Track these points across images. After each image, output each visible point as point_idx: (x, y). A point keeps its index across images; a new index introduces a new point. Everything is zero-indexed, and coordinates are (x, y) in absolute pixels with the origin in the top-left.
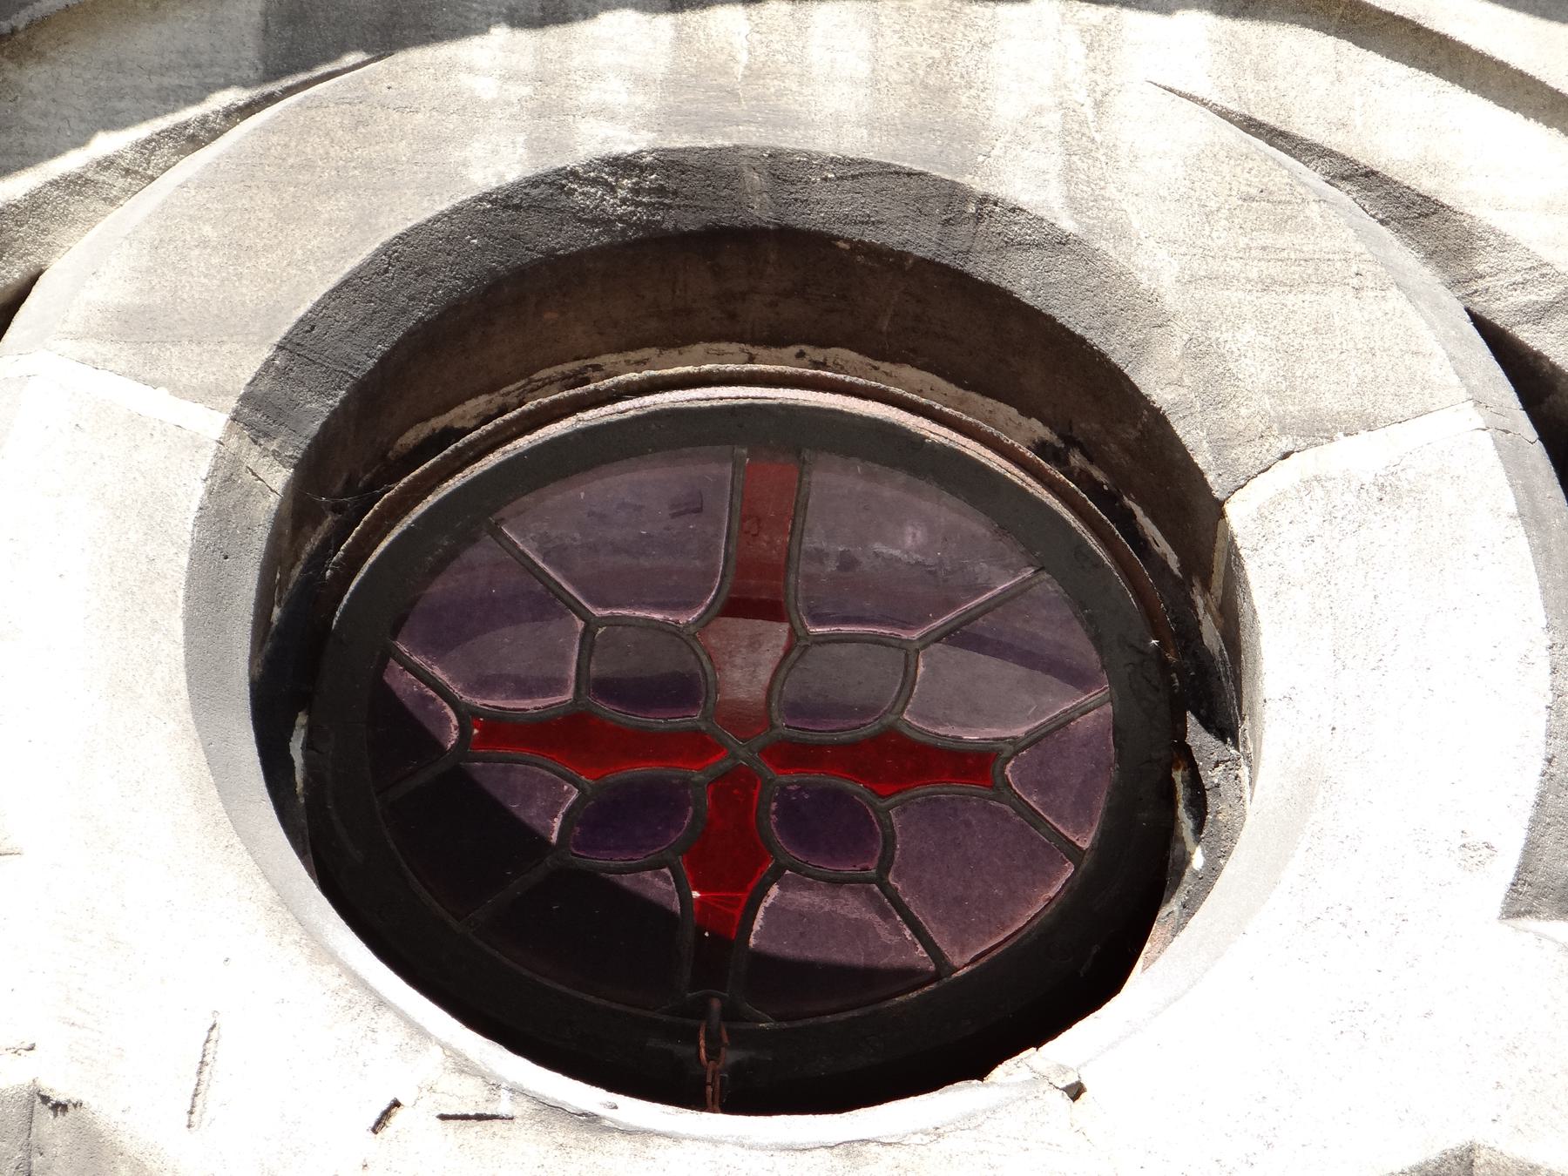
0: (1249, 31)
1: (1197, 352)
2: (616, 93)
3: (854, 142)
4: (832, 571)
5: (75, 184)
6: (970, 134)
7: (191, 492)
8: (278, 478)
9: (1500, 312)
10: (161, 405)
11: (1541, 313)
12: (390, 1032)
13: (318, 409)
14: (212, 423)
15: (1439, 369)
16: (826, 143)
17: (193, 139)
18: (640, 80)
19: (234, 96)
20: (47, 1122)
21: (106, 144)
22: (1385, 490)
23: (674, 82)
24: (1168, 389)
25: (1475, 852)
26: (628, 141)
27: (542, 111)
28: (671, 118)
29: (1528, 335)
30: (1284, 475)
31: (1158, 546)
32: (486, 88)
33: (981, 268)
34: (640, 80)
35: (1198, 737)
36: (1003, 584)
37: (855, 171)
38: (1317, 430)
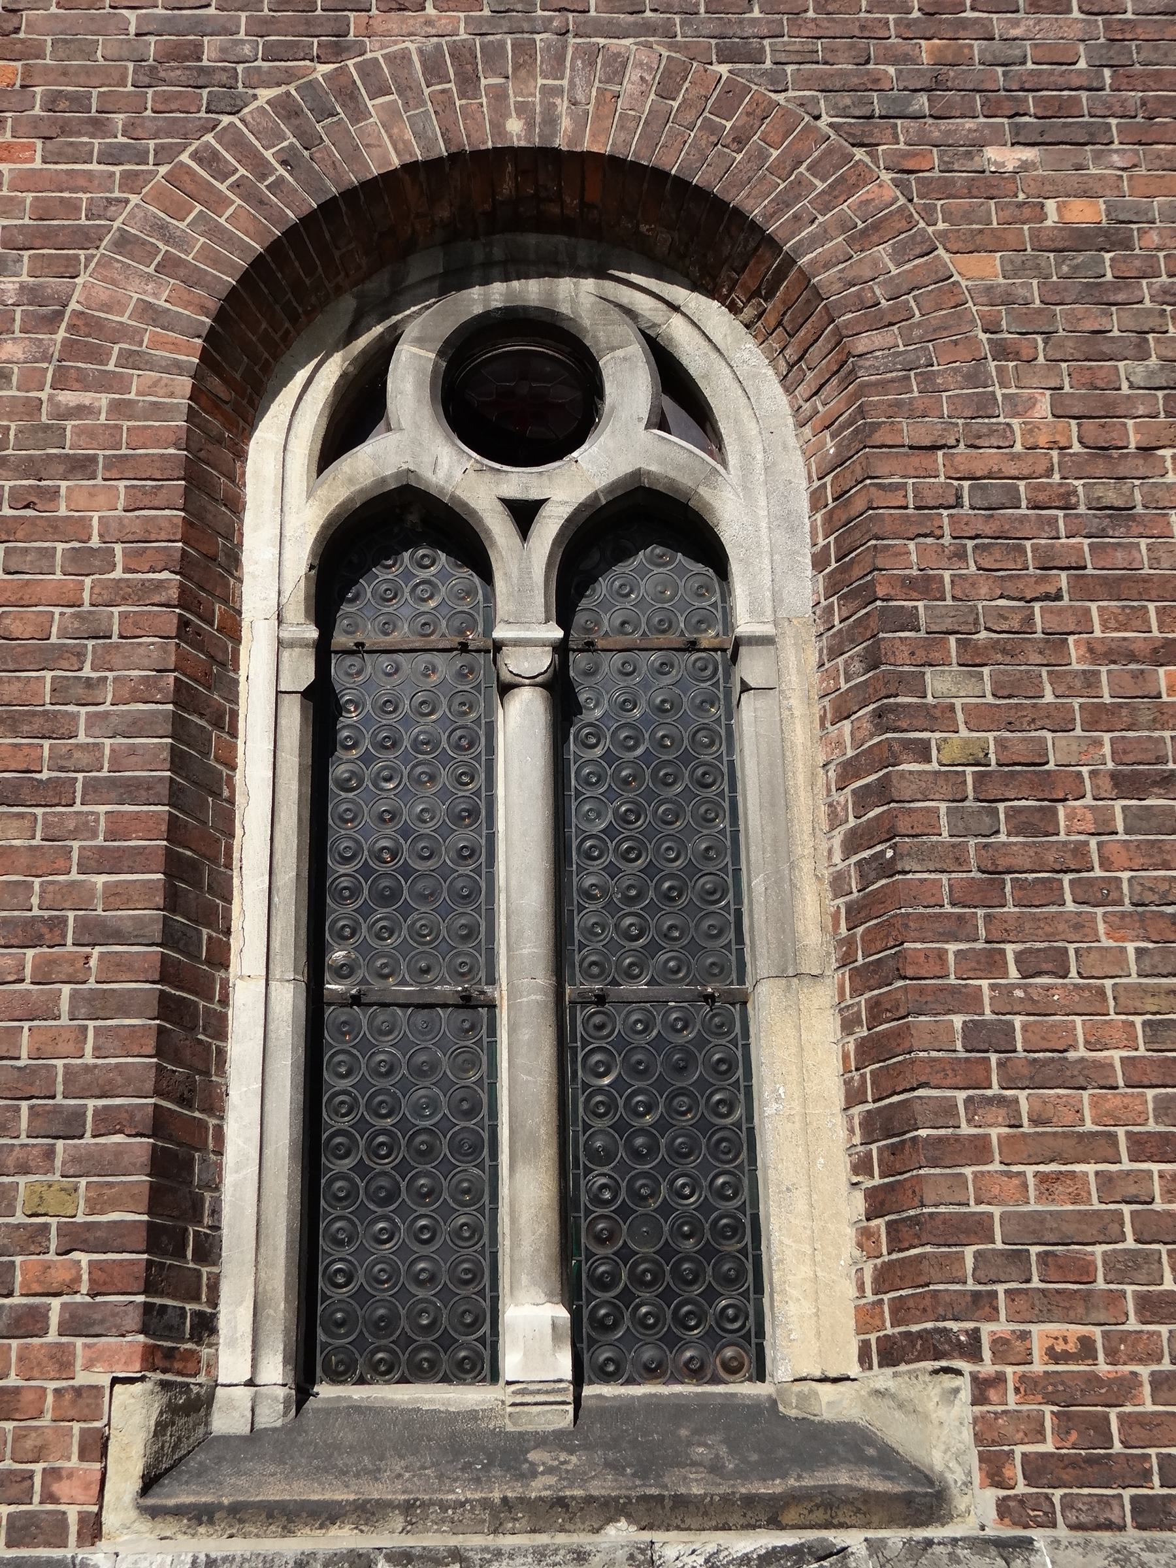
0: (600, 281)
1: (594, 337)
2: (497, 297)
3: (537, 304)
4: (463, 1488)
5: (409, 316)
6: (556, 301)
7: (430, 367)
8: (445, 364)
9: (643, 327)
10: (423, 353)
11: (649, 328)
12: (465, 458)
13: (450, 352)
14: (433, 356)
15: (633, 338)
16: (532, 304)
17: (428, 307)
18: (501, 294)
19: (433, 300)
20: (411, 475)
21: (413, 309)
22: (625, 359)
23: (507, 294)
24: (1069, 1470)
25: (640, 419)
26: (500, 305)
27: (485, 300)
28: (505, 301)
29: (647, 331)
30: (608, 357)
31: (936, 1372)
32: (476, 297)
33: (558, 324)
34: (501, 294)
35: (596, 400)
36: (712, 1394)
37: (537, 308)
38: (613, 349)
